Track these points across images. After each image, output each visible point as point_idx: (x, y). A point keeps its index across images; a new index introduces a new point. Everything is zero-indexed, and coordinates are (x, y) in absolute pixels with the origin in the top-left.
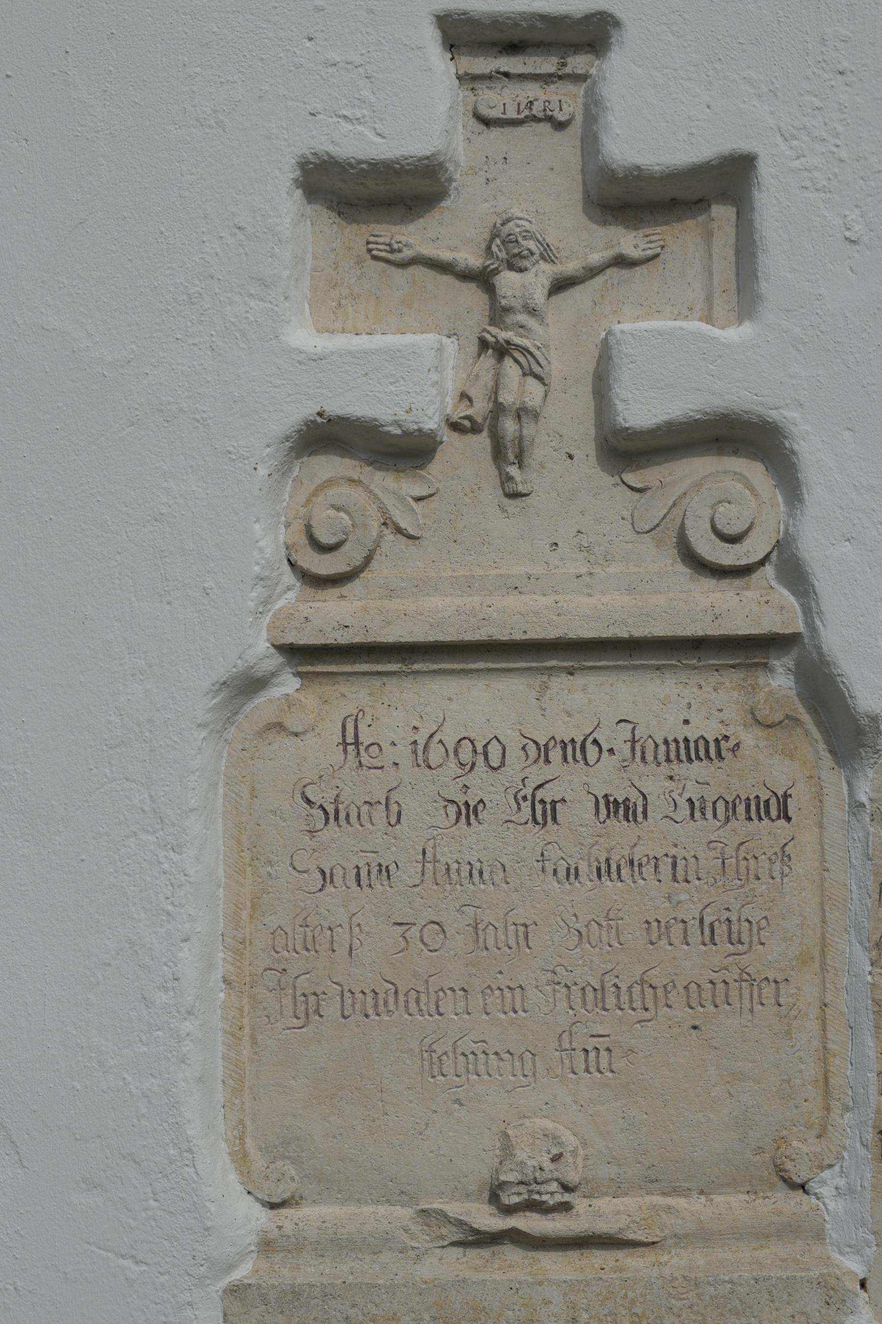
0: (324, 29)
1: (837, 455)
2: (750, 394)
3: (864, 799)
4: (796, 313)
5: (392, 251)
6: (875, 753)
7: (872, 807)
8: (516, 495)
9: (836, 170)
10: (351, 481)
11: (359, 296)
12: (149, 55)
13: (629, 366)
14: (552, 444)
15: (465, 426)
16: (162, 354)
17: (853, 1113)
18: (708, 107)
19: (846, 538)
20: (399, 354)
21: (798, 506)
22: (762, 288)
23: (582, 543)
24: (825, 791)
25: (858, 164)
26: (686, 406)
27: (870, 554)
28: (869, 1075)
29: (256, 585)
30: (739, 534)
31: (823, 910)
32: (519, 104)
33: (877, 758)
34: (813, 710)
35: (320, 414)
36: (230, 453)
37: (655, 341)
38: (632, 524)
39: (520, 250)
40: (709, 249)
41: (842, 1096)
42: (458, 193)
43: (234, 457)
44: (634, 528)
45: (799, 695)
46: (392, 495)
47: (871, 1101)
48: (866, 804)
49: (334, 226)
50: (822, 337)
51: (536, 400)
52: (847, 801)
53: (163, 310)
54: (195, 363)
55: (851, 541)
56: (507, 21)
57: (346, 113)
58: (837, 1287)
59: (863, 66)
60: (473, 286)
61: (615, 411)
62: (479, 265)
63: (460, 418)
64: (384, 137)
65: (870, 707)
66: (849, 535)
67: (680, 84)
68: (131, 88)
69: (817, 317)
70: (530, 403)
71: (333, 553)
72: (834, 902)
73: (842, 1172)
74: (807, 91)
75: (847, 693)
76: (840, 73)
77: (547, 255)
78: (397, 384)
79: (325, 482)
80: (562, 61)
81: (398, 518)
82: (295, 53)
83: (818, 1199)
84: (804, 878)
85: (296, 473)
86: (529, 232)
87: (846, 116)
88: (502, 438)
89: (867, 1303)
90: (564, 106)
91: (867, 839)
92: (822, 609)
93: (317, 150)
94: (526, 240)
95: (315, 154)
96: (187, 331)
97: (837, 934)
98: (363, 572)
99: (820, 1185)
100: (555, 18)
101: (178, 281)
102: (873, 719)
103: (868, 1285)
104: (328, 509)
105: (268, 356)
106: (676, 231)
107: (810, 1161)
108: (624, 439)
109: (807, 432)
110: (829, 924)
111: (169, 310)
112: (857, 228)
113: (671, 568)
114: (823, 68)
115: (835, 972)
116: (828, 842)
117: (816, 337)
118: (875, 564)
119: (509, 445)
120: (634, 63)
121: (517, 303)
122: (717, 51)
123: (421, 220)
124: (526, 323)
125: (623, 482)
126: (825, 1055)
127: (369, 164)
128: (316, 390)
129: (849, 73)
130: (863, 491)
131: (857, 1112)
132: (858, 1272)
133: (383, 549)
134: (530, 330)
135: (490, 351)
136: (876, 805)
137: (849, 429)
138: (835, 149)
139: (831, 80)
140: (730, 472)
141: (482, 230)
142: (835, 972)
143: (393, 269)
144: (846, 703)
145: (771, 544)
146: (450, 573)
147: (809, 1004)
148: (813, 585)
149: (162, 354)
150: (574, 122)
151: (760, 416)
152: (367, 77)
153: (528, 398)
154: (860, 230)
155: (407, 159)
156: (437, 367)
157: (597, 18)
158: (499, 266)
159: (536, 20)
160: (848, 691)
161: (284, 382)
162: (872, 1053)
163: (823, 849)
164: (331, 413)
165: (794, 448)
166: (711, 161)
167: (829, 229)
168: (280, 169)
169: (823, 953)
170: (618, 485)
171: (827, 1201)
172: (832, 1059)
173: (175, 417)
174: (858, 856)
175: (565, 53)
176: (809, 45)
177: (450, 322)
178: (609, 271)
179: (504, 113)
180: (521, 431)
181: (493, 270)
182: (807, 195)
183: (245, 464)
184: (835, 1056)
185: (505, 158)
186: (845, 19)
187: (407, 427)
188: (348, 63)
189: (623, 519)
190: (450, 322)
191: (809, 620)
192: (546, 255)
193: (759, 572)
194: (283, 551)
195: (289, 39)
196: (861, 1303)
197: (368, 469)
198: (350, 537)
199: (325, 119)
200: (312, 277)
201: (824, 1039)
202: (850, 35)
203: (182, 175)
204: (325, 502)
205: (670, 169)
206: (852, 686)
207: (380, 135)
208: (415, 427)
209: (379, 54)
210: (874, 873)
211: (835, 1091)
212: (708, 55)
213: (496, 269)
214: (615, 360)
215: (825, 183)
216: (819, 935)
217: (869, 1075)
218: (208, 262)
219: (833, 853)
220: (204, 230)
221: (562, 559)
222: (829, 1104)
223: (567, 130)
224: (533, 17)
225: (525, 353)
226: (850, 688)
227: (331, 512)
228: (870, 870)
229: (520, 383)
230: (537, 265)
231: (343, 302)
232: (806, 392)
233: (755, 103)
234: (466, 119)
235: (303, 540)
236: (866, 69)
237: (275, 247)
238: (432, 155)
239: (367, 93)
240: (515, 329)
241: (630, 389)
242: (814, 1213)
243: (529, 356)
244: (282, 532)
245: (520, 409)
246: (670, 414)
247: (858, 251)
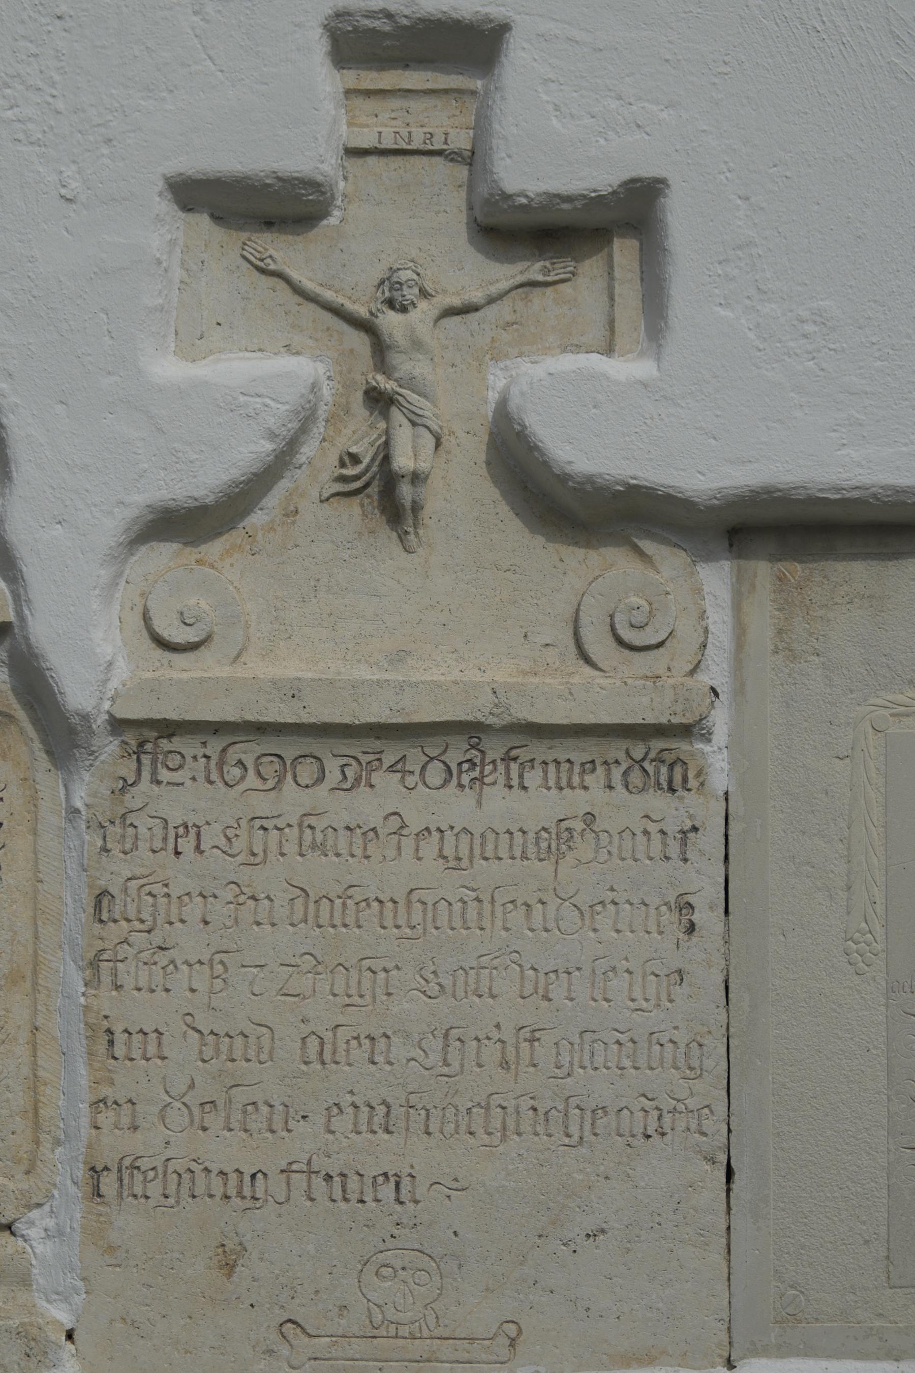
1: (48, 431)
3: (79, 804)
4: (6, 276)
6: (90, 755)
7: (88, 813)
17: (65, 1147)
19: (57, 521)
24: (40, 795)
28: (81, 1106)
31: (36, 924)
33: (93, 760)
34: (29, 707)
41: (53, 1128)
45: (13, 689)
47: (83, 1134)
48: (82, 809)
52: (64, 806)
58: (38, 1338)
59: (83, 10)
65: (80, 704)
66: (60, 517)
69: (29, 280)
72: (48, 917)
73: (52, 1211)
74: (23, 36)
75: (56, 688)
76: (58, 17)
83: (25, 1241)
84: (15, 889)
87: (63, 64)
89: (73, 1356)
91: (83, 847)
92: (30, 596)
97: (50, 951)
99: (27, 1226)
102: (83, 717)
103: (75, 1337)
107: (17, 1199)
109: (17, 405)
110: (41, 939)
112: (74, 185)
114: (39, 12)
115: (47, 993)
116: (42, 850)
117: (27, 302)
118: (88, 549)
126: (35, 1083)
130: (76, 470)
131: (68, 1146)
132: (65, 1321)
136: (93, 811)
137: (62, 402)
138: (51, 100)
139: (48, 24)
142: (47, 993)
144: (56, 699)
147: (19, 1027)
148: (21, 571)
154: (76, 188)
160: (57, 685)
162: (84, 1082)
163: (37, 858)
167: (42, 185)
169: (35, 972)
171: (34, 1244)
172: (42, 1088)
174: (74, 866)
182: (20, 149)
184: (46, 1084)
191: (18, 608)
196: (65, 1356)
201: (35, 1066)
206: (61, 681)
210: (89, 886)
211: (45, 1123)
215: (40, 136)
216: (31, 952)
217: (81, 1106)
219: (48, 863)
222: (39, 1137)
226: (59, 684)
228: (85, 882)
232: (15, 362)
236: (86, 14)
242: (20, 1256)
247: (74, 210)
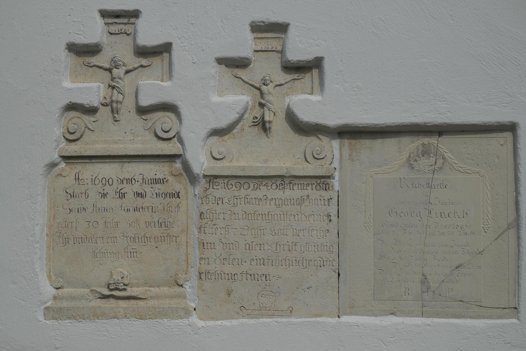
9: (191, 46)
35: (70, 102)
77: (124, 65)
85: (65, 115)
90: (129, 30)
100: (126, 11)
109: (183, 107)
134: (119, 83)
135: (111, 87)
137: (193, 107)
138: (190, 42)
143: (89, 67)
151: (172, 103)
178: (139, 68)
179: (115, 32)
198: (77, 131)
214: (139, 90)
221: (127, 136)
227: (73, 125)
231: (77, 75)
235: (67, 131)
238: (97, 43)
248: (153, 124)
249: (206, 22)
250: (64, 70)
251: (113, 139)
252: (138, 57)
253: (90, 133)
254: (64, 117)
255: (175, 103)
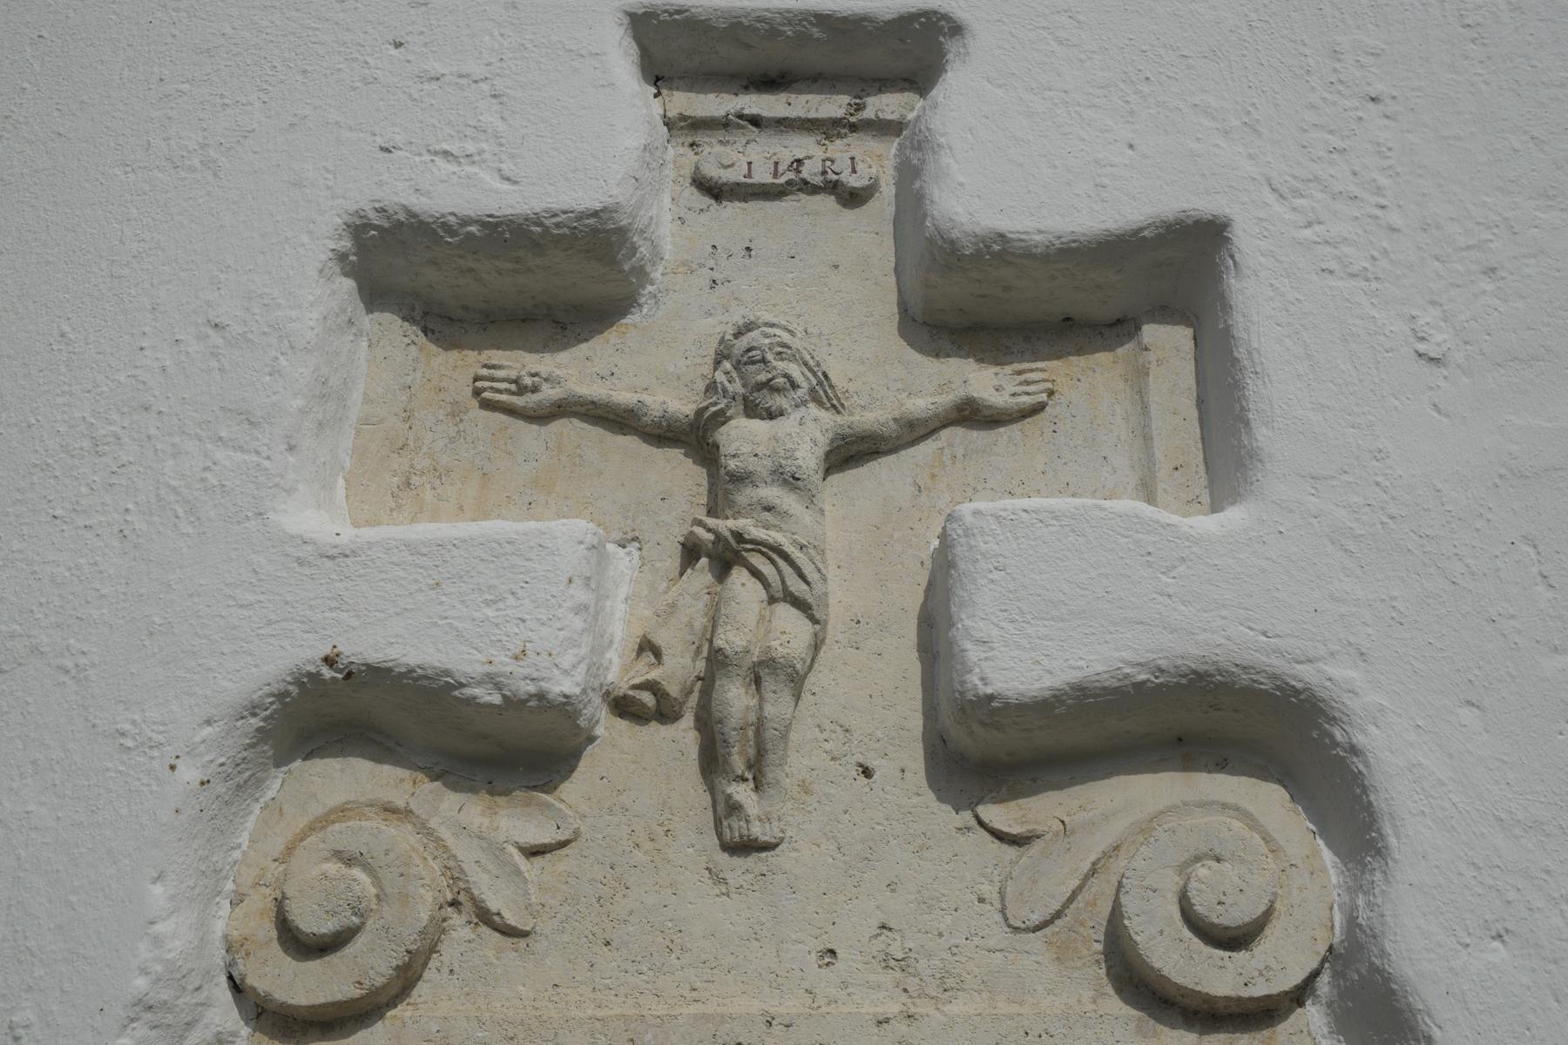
0: (425, 29)
2: (1251, 633)
4: (1334, 483)
5: (522, 390)
8: (744, 847)
9: (1385, 244)
10: (390, 810)
11: (449, 471)
12: (99, 67)
13: (990, 576)
14: (828, 746)
15: (644, 705)
16: (16, 545)
18: (1131, 146)
20: (508, 548)
21: (1376, 865)
22: (1259, 438)
23: (891, 950)
25: (1425, 235)
26: (1116, 654)
27: (1552, 967)
29: (132, 1020)
30: (1246, 925)
32: (776, 163)
35: (329, 661)
36: (123, 734)
37: (1045, 530)
38: (1003, 911)
39: (770, 376)
40: (1142, 397)
42: (656, 303)
43: (130, 743)
44: (1006, 919)
46: (476, 841)
49: (413, 348)
50: (1392, 525)
51: (794, 644)
53: (36, 466)
54: (82, 561)
55: (1506, 938)
56: (758, 25)
57: (447, 148)
59: (1413, 89)
60: (676, 454)
61: (963, 663)
62: (688, 412)
63: (635, 687)
64: (516, 183)
66: (1499, 926)
67: (1076, 112)
68: (56, 114)
70: (780, 649)
71: (327, 958)
76: (1373, 99)
77: (824, 394)
78: (501, 605)
79: (331, 812)
80: (858, 101)
81: (484, 889)
82: (366, 63)
85: (271, 794)
86: (790, 348)
87: (1390, 162)
88: (720, 722)
90: (860, 167)
93: (386, 203)
94: (782, 360)
95: (382, 210)
96: (78, 503)
98: (395, 1006)
100: (845, 19)
101: (77, 415)
104: (327, 860)
105: (235, 549)
106: (1075, 369)
108: (983, 724)
109: (1382, 709)
111: (48, 465)
113: (1094, 1007)
114: (1339, 92)
117: (1379, 526)
119: (733, 736)
120: (990, 82)
121: (761, 468)
122: (1141, 67)
123: (584, 346)
124: (777, 501)
125: (981, 823)
127: (483, 224)
128: (326, 614)
129: (1388, 101)
133: (446, 958)
134: (785, 515)
135: (704, 561)
137: (1470, 704)
138: (1378, 212)
140: (1212, 803)
141: (699, 360)
143: (520, 424)
145: (1318, 953)
146: (590, 1012)
149: (16, 545)
150: (877, 194)
151: (1274, 677)
152: (494, 96)
153: (778, 642)
154: (1445, 341)
155: (555, 215)
156: (589, 579)
157: (921, 24)
158: (728, 406)
159: (811, 23)
161: (262, 598)
164: (353, 659)
165: (1354, 741)
166: (1141, 229)
167: (1382, 338)
168: (310, 232)
170: (969, 829)
173: (20, 664)
175: (862, 90)
176: (1311, 61)
177: (626, 518)
178: (945, 434)
179: (749, 175)
180: (761, 708)
181: (716, 414)
183: (152, 758)
185: (748, 249)
186: (1370, 25)
187: (513, 688)
188: (460, 76)
189: (981, 900)
190: (626, 518)
192: (821, 392)
193: (1292, 1018)
194: (218, 957)
195: (359, 44)
197: (429, 787)
198: (370, 922)
199: (407, 158)
200: (358, 433)
202: (1384, 47)
203: (122, 242)
204: (322, 846)
205: (1063, 240)
207: (508, 179)
208: (532, 688)
209: (519, 63)
212: (1125, 72)
213: (722, 412)
214: (962, 565)
215: (1366, 264)
218: (144, 383)
220: (147, 329)
221: (845, 985)
223: (864, 207)
224: (805, 20)
225: (775, 556)
227: (333, 867)
229: (762, 617)
230: (803, 409)
231: (415, 480)
233: (1218, 142)
234: (678, 188)
235: (269, 931)
236: (1419, 94)
237: (281, 358)
238: (604, 209)
239: (492, 119)
240: (755, 515)
241: (995, 620)
243: (781, 563)
244: (221, 913)
245: (761, 663)
246: (1080, 668)
247: (1445, 378)
248: (1086, 879)
249: (1483, 87)
250: (303, 412)
251: (710, 1009)
252: (937, 356)
253: (491, 953)
254: (257, 810)
255: (1306, 675)
